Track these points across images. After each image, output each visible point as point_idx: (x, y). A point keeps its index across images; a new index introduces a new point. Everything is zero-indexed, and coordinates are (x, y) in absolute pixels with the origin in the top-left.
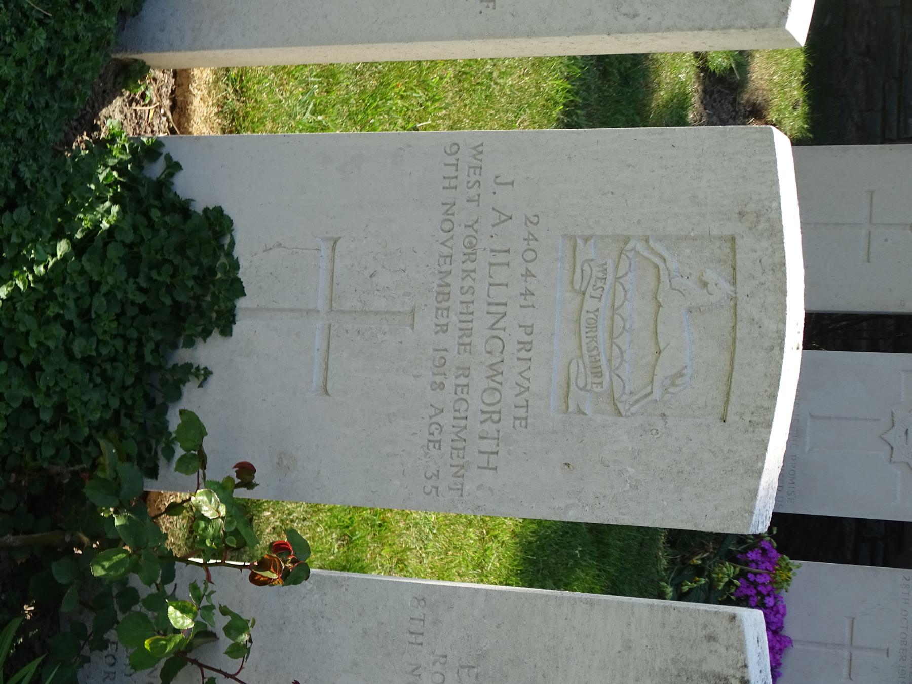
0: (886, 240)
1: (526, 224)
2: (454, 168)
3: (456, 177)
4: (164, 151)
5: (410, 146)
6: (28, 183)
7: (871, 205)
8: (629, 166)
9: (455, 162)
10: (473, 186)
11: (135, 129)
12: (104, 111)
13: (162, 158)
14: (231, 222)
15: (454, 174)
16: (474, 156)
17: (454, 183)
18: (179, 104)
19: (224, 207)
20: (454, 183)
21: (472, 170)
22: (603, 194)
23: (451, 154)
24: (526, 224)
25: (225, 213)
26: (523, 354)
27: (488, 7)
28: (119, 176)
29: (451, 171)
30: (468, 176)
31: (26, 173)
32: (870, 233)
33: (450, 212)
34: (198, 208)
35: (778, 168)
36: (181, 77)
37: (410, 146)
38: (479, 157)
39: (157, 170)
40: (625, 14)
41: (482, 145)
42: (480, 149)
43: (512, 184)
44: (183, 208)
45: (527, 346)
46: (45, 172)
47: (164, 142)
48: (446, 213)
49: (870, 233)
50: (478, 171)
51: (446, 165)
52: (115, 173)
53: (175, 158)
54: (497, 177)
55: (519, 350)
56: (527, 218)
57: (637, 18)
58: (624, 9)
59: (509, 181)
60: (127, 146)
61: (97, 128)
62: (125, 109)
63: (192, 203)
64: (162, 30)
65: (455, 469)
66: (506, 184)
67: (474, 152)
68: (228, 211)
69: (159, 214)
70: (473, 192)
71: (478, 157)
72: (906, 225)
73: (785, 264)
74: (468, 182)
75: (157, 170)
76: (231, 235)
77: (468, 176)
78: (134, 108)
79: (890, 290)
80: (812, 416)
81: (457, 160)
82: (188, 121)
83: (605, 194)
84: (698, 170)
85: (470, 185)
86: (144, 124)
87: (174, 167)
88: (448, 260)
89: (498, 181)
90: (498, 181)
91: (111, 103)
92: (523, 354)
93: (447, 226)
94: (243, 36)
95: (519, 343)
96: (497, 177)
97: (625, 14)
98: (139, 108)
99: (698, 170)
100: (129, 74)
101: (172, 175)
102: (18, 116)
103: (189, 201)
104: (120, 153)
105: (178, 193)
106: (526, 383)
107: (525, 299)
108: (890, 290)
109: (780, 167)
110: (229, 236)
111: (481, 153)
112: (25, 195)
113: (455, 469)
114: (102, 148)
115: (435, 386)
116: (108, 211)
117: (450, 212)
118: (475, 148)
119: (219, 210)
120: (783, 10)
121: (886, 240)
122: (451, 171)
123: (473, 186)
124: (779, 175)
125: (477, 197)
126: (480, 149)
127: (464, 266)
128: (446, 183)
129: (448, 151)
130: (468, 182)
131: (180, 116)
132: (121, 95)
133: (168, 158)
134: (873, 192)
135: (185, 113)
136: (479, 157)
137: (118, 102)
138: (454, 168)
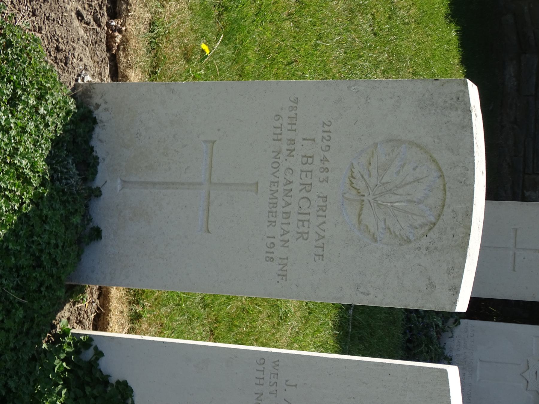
0: (524, 258)
1: (322, 141)
2: (262, 373)
3: (263, 378)
4: (94, 344)
5: (236, 357)
6: (13, 390)
7: (516, 237)
8: (364, 383)
9: (262, 369)
10: (273, 384)
11: (77, 318)
12: (59, 314)
13: (92, 348)
14: (132, 391)
15: (262, 376)
16: (274, 367)
17: (262, 382)
18: (103, 292)
19: (128, 381)
20: (262, 382)
21: (272, 375)
22: (349, 398)
23: (260, 364)
24: (322, 141)
25: (129, 384)
26: (321, 213)
27: (282, 279)
28: (67, 365)
29: (260, 374)
30: (270, 378)
31: (12, 385)
32: (515, 254)
33: (259, 399)
34: (113, 380)
35: (451, 394)
36: (104, 295)
37: (236, 357)
38: (277, 368)
39: (89, 354)
40: (362, 293)
41: (278, 361)
42: (277, 363)
43: (296, 386)
44: (105, 381)
45: (323, 208)
46: (23, 379)
47: (93, 338)
48: (275, 157)
49: (515, 254)
50: (276, 376)
51: (257, 370)
52: (64, 364)
53: (100, 348)
54: (287, 381)
55: (318, 211)
56: (324, 123)
57: (369, 296)
58: (362, 290)
59: (294, 384)
60: (72, 342)
61: (54, 327)
62: (71, 309)
63: (109, 378)
64: (93, 272)
65: (281, 266)
66: (292, 386)
67: (274, 365)
68: (130, 384)
69: (90, 389)
70: (273, 388)
71: (276, 368)
72: (536, 250)
73: (469, 235)
74: (270, 382)
75: (89, 354)
76: (132, 399)
77: (270, 378)
78: (76, 306)
79: (527, 288)
80: (480, 361)
81: (264, 368)
82: (109, 303)
83: (349, 398)
84: (404, 390)
85: (271, 384)
86: (82, 313)
87: (99, 354)
88: (276, 184)
89: (288, 383)
90: (288, 383)
91: (62, 309)
92: (321, 213)
93: (276, 165)
94: (140, 280)
95: (318, 206)
96: (287, 381)
97: (362, 293)
98: (79, 305)
99: (404, 390)
100: (74, 291)
101: (97, 359)
102: (7, 357)
103: (109, 376)
104: (68, 347)
105: (101, 370)
106: (322, 233)
107: (324, 163)
108: (527, 288)
109: (472, 105)
110: (131, 399)
111: (278, 365)
112: (11, 395)
113: (281, 266)
114: (59, 338)
115: (268, 259)
116: (59, 394)
117: (259, 399)
118: (274, 362)
119: (125, 383)
120: (454, 301)
121: (524, 258)
122: (260, 374)
123: (273, 384)
124: (451, 398)
125: (275, 392)
126: (277, 363)
127: (285, 188)
128: (275, 137)
129: (258, 362)
130: (270, 382)
131: (104, 300)
132: (70, 301)
133: (96, 348)
134: (517, 229)
135: (107, 299)
136: (277, 368)
137: (67, 306)
138: (262, 373)
